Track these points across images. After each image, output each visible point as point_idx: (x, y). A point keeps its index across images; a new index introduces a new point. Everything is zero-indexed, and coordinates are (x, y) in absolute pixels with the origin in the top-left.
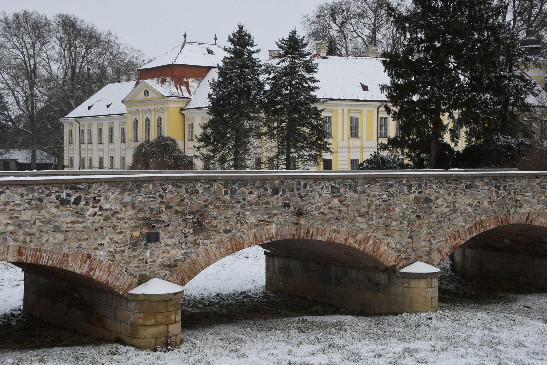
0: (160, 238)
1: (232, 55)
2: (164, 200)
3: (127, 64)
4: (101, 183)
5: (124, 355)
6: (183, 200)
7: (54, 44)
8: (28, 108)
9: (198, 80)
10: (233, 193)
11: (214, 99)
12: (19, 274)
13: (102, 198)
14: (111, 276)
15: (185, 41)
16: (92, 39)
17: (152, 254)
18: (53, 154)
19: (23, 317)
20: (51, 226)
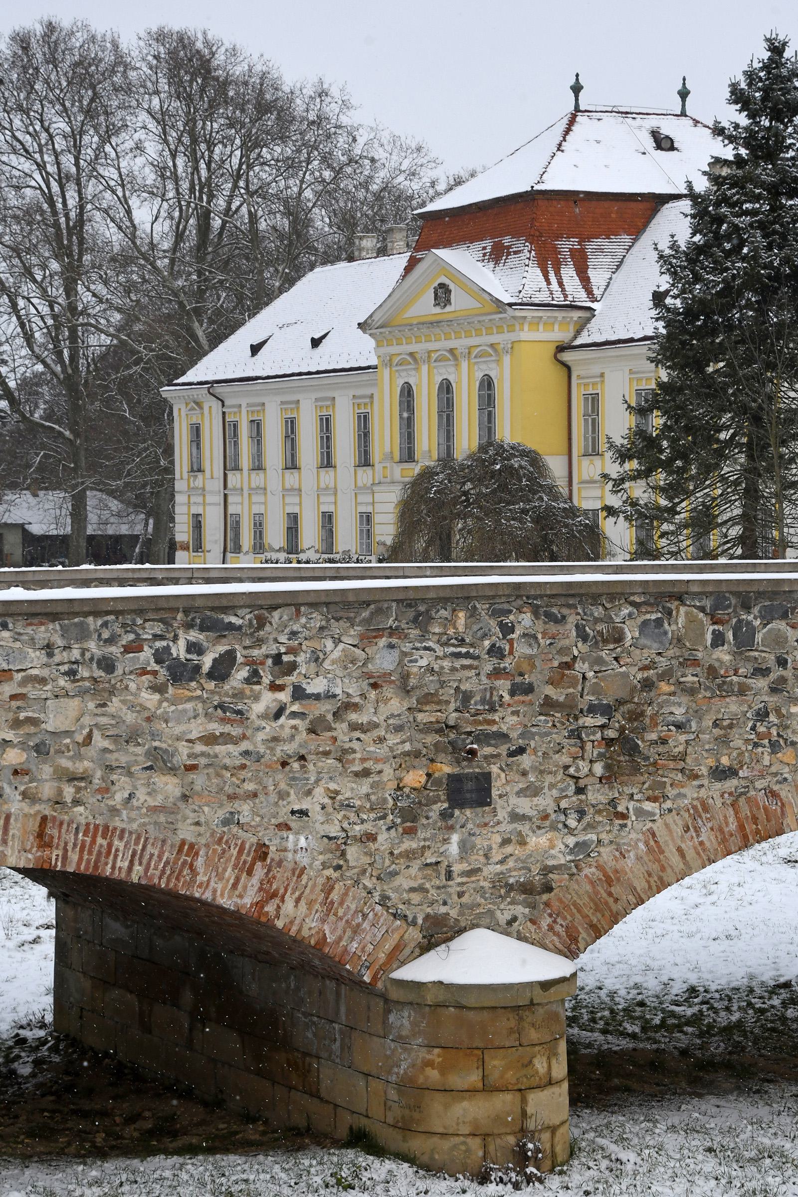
0: (495, 793)
1: (743, 152)
2: (507, 663)
3: (378, 197)
4: (298, 606)
5: (379, 1189)
6: (568, 666)
7: (140, 135)
8: (59, 354)
9: (616, 245)
10: (744, 639)
11: (675, 311)
12: (38, 905)
13: (301, 658)
14: (332, 918)
15: (577, 109)
16: (263, 112)
17: (464, 846)
18: (139, 504)
19: (54, 1049)
20: (139, 750)
